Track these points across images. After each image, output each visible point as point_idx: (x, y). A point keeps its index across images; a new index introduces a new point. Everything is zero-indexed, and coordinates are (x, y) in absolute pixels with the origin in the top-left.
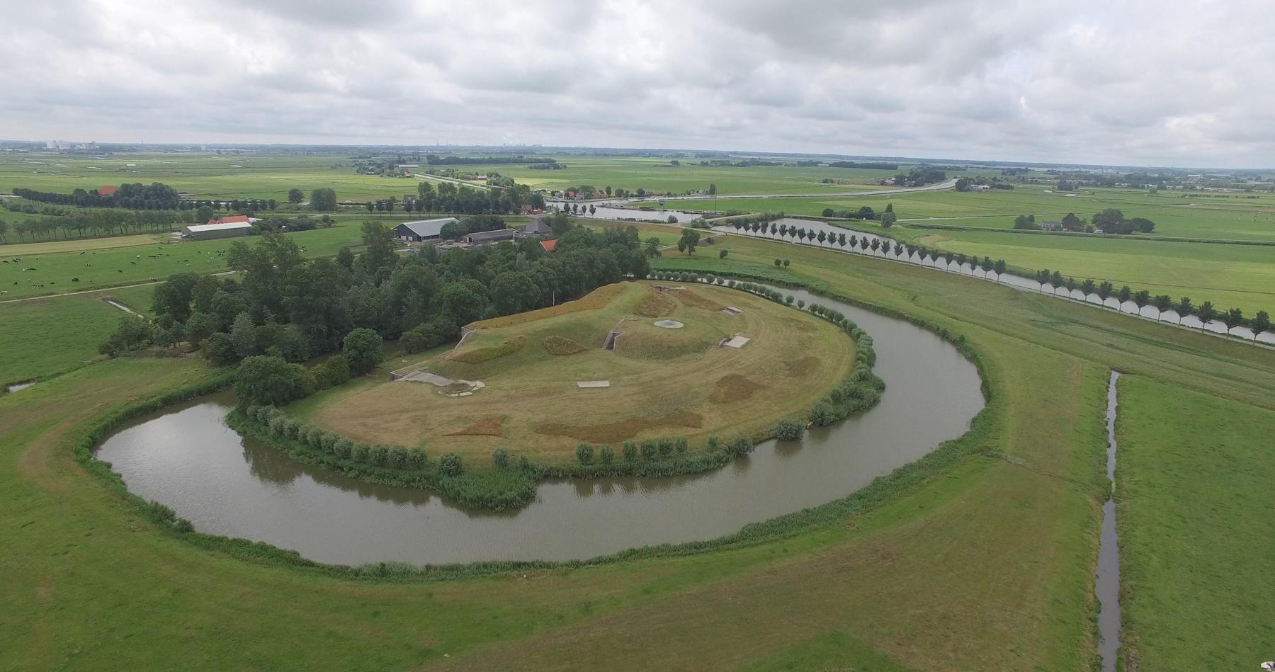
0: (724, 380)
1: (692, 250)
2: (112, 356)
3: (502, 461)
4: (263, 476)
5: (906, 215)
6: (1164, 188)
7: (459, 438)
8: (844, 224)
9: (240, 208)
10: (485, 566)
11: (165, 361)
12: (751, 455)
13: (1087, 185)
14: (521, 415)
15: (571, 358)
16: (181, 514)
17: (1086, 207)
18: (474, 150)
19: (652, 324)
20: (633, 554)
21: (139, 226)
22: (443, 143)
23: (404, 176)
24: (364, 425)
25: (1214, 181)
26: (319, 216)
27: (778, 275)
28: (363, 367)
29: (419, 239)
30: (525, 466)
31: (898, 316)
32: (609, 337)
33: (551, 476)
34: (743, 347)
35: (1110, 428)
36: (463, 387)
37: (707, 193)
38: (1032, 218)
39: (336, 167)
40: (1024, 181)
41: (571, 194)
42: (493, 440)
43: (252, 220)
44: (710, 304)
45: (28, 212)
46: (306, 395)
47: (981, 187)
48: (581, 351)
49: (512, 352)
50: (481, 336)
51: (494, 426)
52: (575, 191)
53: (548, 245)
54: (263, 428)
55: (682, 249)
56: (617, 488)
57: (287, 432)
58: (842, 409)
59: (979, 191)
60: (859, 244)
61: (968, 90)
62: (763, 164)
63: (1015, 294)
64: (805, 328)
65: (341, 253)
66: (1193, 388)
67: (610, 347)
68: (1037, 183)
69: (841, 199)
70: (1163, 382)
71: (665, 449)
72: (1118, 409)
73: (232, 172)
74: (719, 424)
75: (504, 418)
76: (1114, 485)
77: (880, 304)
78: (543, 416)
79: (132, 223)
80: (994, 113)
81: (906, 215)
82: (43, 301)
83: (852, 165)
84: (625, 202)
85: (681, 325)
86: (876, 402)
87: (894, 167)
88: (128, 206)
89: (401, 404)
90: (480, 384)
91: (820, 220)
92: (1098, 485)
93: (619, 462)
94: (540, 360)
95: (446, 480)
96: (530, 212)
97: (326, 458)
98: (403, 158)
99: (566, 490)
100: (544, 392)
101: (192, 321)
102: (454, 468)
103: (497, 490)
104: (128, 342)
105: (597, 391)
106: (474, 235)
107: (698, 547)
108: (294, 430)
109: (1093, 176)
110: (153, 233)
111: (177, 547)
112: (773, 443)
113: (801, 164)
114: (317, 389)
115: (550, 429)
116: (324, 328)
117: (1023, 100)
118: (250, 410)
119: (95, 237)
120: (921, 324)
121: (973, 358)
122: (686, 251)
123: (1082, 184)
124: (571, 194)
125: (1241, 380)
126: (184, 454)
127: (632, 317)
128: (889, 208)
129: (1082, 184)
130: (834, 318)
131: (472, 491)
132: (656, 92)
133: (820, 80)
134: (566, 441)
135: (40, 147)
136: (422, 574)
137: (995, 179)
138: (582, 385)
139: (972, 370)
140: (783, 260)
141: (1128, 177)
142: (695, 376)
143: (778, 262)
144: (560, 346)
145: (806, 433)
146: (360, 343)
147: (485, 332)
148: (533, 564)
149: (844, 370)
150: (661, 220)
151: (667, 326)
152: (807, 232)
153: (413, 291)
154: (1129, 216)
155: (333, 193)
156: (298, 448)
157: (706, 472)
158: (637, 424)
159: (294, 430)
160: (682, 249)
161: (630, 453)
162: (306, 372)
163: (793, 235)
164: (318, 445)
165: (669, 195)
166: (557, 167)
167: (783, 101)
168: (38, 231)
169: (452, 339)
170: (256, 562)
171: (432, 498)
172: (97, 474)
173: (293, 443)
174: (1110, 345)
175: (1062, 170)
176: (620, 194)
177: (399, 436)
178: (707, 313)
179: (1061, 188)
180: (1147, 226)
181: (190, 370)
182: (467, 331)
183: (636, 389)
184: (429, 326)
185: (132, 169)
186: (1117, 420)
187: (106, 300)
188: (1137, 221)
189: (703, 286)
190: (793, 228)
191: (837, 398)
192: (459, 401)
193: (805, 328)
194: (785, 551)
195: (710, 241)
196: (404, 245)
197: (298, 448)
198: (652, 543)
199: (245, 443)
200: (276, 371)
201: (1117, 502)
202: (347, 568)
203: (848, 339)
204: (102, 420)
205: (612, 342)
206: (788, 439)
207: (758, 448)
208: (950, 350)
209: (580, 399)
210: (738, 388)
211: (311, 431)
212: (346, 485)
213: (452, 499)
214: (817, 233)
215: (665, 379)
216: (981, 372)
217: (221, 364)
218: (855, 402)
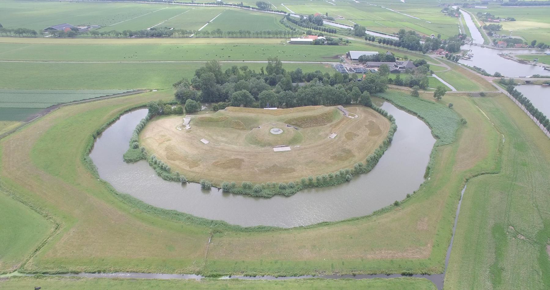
1: (439, 98)
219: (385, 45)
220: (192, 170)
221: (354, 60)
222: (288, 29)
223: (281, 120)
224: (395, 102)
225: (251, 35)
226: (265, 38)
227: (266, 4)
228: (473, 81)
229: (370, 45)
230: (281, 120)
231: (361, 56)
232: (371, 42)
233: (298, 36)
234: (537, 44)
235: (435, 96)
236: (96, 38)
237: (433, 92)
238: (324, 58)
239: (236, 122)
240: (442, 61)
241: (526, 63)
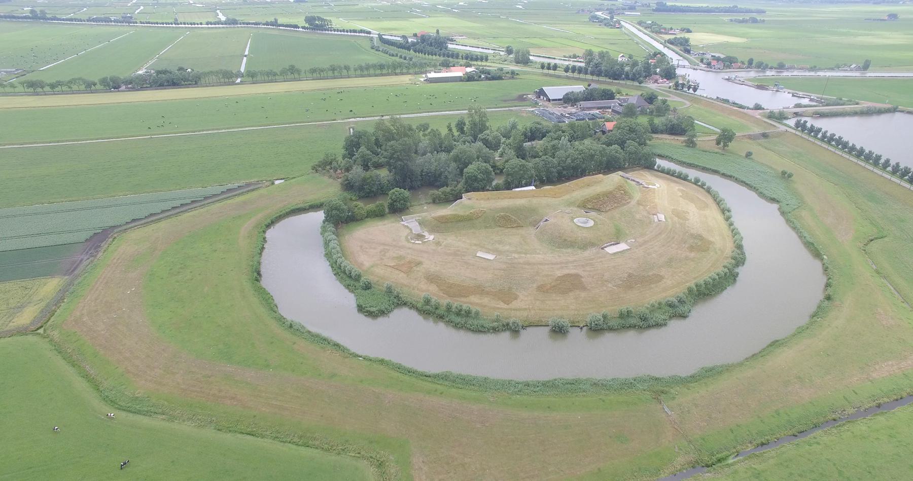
1: (725, 145)
7: (389, 269)
14: (430, 265)
29: (549, 100)
37: (858, 69)
74: (524, 305)
165: (813, 69)
183: (504, 266)
190: (840, 138)
219: (576, 75)
220: (510, 306)
221: (554, 100)
222: (397, 59)
223: (570, 204)
224: (675, 157)
225: (352, 72)
226: (376, 76)
227: (323, 20)
228: (733, 117)
229: (551, 76)
230: (570, 204)
231: (567, 94)
232: (551, 72)
233: (428, 69)
234: (754, 65)
235: (718, 143)
236: (37, 94)
237: (715, 137)
238: (505, 101)
239: (502, 217)
240: (670, 92)
241: (767, 89)
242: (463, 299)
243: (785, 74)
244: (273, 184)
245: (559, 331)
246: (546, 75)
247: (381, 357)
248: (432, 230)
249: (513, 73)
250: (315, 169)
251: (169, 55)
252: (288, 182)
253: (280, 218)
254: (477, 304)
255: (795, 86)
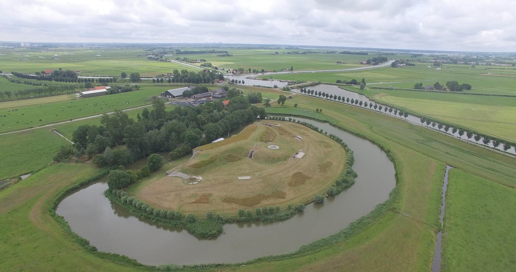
0: (295, 175)
1: (283, 103)
2: (59, 161)
3: (210, 217)
4: (119, 215)
5: (370, 81)
6: (478, 64)
7: (194, 205)
8: (345, 87)
9: (103, 82)
10: (205, 266)
11: (79, 164)
12: (304, 210)
13: (446, 63)
14: (217, 193)
15: (236, 163)
16: (92, 244)
17: (443, 76)
18: (195, 46)
19: (267, 147)
20: (260, 260)
21: (63, 91)
22: (182, 42)
23: (166, 61)
24: (157, 198)
25: (500, 60)
26: (134, 84)
27: (317, 116)
28: (155, 169)
29: (174, 97)
30: (219, 218)
31: (364, 138)
32: (250, 152)
33: (228, 221)
34: (302, 157)
35: (443, 196)
36: (194, 180)
37: (289, 70)
38: (421, 84)
39: (139, 56)
40: (419, 61)
41: (235, 72)
42: (206, 205)
43: (108, 87)
44: (290, 134)
45: (18, 83)
46: (134, 182)
47: (402, 65)
48: (240, 159)
49: (213, 161)
50: (200, 154)
51: (205, 199)
52: (236, 71)
53: (226, 102)
54: (119, 199)
55: (279, 103)
56: (254, 226)
57: (128, 202)
58: (339, 188)
59: (401, 67)
60: (350, 101)
61: (397, 20)
62: (313, 53)
63: (412, 127)
64: (327, 146)
65: (144, 111)
66: (478, 175)
67: (251, 157)
68: (425, 62)
69: (344, 72)
70: (467, 172)
71: (271, 211)
72: (448, 186)
73: (97, 58)
74: (293, 197)
75: (210, 195)
76: (442, 225)
77: (358, 132)
78: (225, 194)
79: (60, 90)
80: (408, 30)
81: (370, 81)
82: (29, 132)
83: (349, 53)
84: (256, 75)
85: (278, 147)
86: (353, 183)
87: (366, 54)
88: (57, 80)
89: (170, 187)
90: (200, 178)
91: (335, 85)
92: (436, 225)
93: (255, 216)
94: (223, 164)
95: (189, 225)
96: (218, 82)
97: (144, 214)
98: (167, 50)
99: (235, 226)
100: (225, 182)
101: (88, 149)
102: (192, 220)
103: (207, 228)
104: (64, 156)
105: (246, 180)
106: (196, 96)
107: (283, 257)
108: (131, 201)
109: (449, 58)
110: (68, 94)
111: (91, 257)
112: (313, 204)
113: (328, 53)
114: (138, 179)
115: (228, 200)
116: (139, 150)
117: (421, 24)
118: (114, 191)
119: (45, 96)
120: (373, 142)
121: (393, 160)
122: (281, 103)
123: (444, 63)
124: (235, 72)
125: (497, 172)
126: (91, 207)
127: (259, 143)
128: (363, 80)
129: (444, 63)
130: (339, 141)
131: (200, 230)
132: (268, 22)
133: (336, 16)
134: (234, 205)
135: (18, 45)
136: (182, 270)
137: (408, 60)
138: (240, 178)
139: (392, 165)
140: (319, 109)
141: (464, 59)
142: (283, 172)
143: (317, 110)
144: (231, 157)
145: (325, 199)
146: (154, 160)
147: (201, 152)
148: (223, 265)
149: (341, 167)
150: (271, 85)
151: (273, 147)
152: (329, 95)
153: (173, 134)
154: (460, 83)
155: (139, 74)
156: (133, 209)
157: (287, 219)
158: (261, 197)
159: (131, 201)
160: (279, 103)
161: (258, 213)
162: (134, 172)
163: (324, 96)
164: (140, 208)
165: (274, 71)
166: (228, 56)
167: (321, 25)
168: (24, 95)
169: (188, 153)
170: (121, 265)
171: (184, 230)
172: (59, 222)
173: (131, 207)
174: (447, 153)
175: (436, 54)
176: (255, 72)
177: (169, 204)
178: (289, 139)
179: (435, 65)
180: (468, 87)
181: (88, 170)
182: (195, 151)
183: (261, 180)
184: (180, 149)
185: (57, 57)
186: (447, 192)
187: (52, 131)
188: (464, 85)
189: (288, 123)
190: (324, 93)
191: (338, 184)
192: (192, 186)
193: (327, 146)
194: (315, 259)
195: (290, 98)
196: (168, 100)
197: (133, 209)
198: (266, 255)
199: (112, 203)
200: (124, 177)
201: (443, 233)
202: (155, 267)
203: (344, 151)
204: (58, 194)
205: (251, 154)
206: (319, 203)
207: (307, 207)
208: (384, 154)
209: (239, 185)
210: (299, 179)
211: (138, 203)
212: (151, 224)
213: (192, 233)
214: (334, 96)
215: (272, 175)
216: (395, 167)
217: (100, 167)
218: (345, 185)
229: (160, 86)
242: (259, 205)
243: (265, 74)
244: (21, 179)
245: (319, 203)
246: (158, 86)
247: (257, 258)
248: (197, 174)
249: (136, 86)
250: (58, 159)
251: (387, 91)
252: (34, 176)
253: (60, 200)
254: (269, 204)
255: (281, 79)
